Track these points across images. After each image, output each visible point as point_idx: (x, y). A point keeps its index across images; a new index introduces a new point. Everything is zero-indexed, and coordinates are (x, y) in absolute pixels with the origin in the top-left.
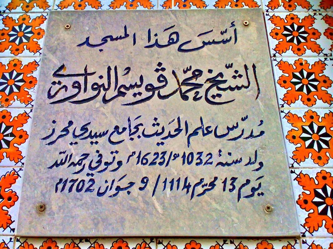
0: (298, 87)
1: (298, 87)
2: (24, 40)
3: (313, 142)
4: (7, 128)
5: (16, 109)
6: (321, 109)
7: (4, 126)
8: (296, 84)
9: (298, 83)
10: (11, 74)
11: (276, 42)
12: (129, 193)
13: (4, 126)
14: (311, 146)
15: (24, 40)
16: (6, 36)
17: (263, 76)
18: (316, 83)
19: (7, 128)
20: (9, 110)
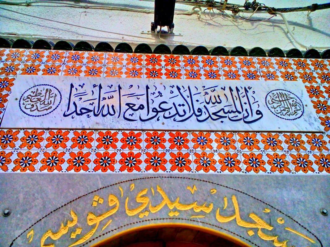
0: (232, 160)
1: (232, 160)
2: (6, 136)
3: (201, 142)
4: (3, 158)
5: (8, 150)
6: (326, 153)
7: (2, 157)
8: (184, 161)
9: (226, 162)
10: (58, 143)
11: (219, 73)
12: (16, 99)
13: (2, 157)
14: (247, 144)
15: (6, 136)
16: (298, 148)
17: (54, 199)
18: (225, 161)
19: (3, 158)
20: (31, 151)
